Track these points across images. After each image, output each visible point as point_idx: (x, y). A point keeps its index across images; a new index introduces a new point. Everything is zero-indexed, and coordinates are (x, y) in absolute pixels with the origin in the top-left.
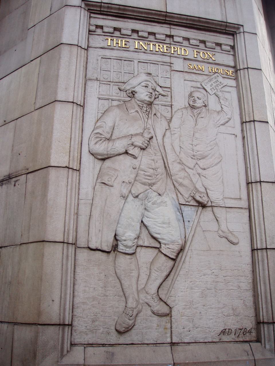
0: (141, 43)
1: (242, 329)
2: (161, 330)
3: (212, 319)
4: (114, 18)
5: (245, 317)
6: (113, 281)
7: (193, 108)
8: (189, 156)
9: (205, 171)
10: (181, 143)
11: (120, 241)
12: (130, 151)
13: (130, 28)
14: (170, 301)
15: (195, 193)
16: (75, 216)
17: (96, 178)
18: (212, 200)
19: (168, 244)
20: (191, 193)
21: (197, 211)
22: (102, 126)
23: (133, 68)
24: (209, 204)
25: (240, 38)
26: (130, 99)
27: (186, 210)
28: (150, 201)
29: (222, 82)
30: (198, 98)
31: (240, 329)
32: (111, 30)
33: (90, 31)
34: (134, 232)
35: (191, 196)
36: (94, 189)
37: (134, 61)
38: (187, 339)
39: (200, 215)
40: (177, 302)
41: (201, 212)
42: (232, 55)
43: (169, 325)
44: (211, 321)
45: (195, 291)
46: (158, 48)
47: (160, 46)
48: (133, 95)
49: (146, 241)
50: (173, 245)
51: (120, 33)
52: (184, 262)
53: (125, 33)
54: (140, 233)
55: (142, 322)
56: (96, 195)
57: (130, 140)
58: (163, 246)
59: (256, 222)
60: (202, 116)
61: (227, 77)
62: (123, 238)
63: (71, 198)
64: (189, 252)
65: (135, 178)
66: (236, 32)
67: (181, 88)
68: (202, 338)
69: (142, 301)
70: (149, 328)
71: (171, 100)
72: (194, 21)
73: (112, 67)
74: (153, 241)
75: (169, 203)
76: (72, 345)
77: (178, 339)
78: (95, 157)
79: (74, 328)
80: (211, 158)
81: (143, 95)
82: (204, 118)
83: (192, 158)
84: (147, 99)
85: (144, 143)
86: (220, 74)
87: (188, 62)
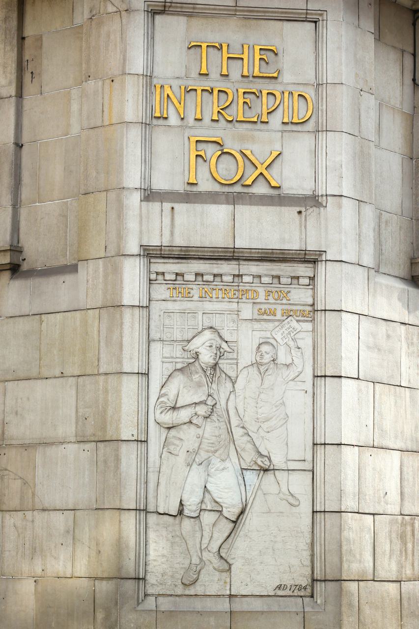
2: (222, 583)
3: (268, 575)
13: (194, 272)
16: (145, 485)
17: (162, 446)
18: (274, 464)
19: (229, 508)
22: (167, 393)
23: (197, 322)
24: (272, 467)
25: (321, 267)
30: (265, 352)
32: (173, 277)
33: (150, 280)
40: (236, 559)
41: (262, 476)
43: (228, 580)
44: (268, 577)
50: (234, 508)
56: (162, 463)
58: (224, 509)
61: (303, 319)
62: (188, 503)
63: (141, 469)
67: (246, 340)
72: (267, 253)
75: (231, 468)
76: (146, 595)
79: (147, 582)
81: (207, 357)
83: (256, 421)
86: (294, 316)
87: (258, 306)
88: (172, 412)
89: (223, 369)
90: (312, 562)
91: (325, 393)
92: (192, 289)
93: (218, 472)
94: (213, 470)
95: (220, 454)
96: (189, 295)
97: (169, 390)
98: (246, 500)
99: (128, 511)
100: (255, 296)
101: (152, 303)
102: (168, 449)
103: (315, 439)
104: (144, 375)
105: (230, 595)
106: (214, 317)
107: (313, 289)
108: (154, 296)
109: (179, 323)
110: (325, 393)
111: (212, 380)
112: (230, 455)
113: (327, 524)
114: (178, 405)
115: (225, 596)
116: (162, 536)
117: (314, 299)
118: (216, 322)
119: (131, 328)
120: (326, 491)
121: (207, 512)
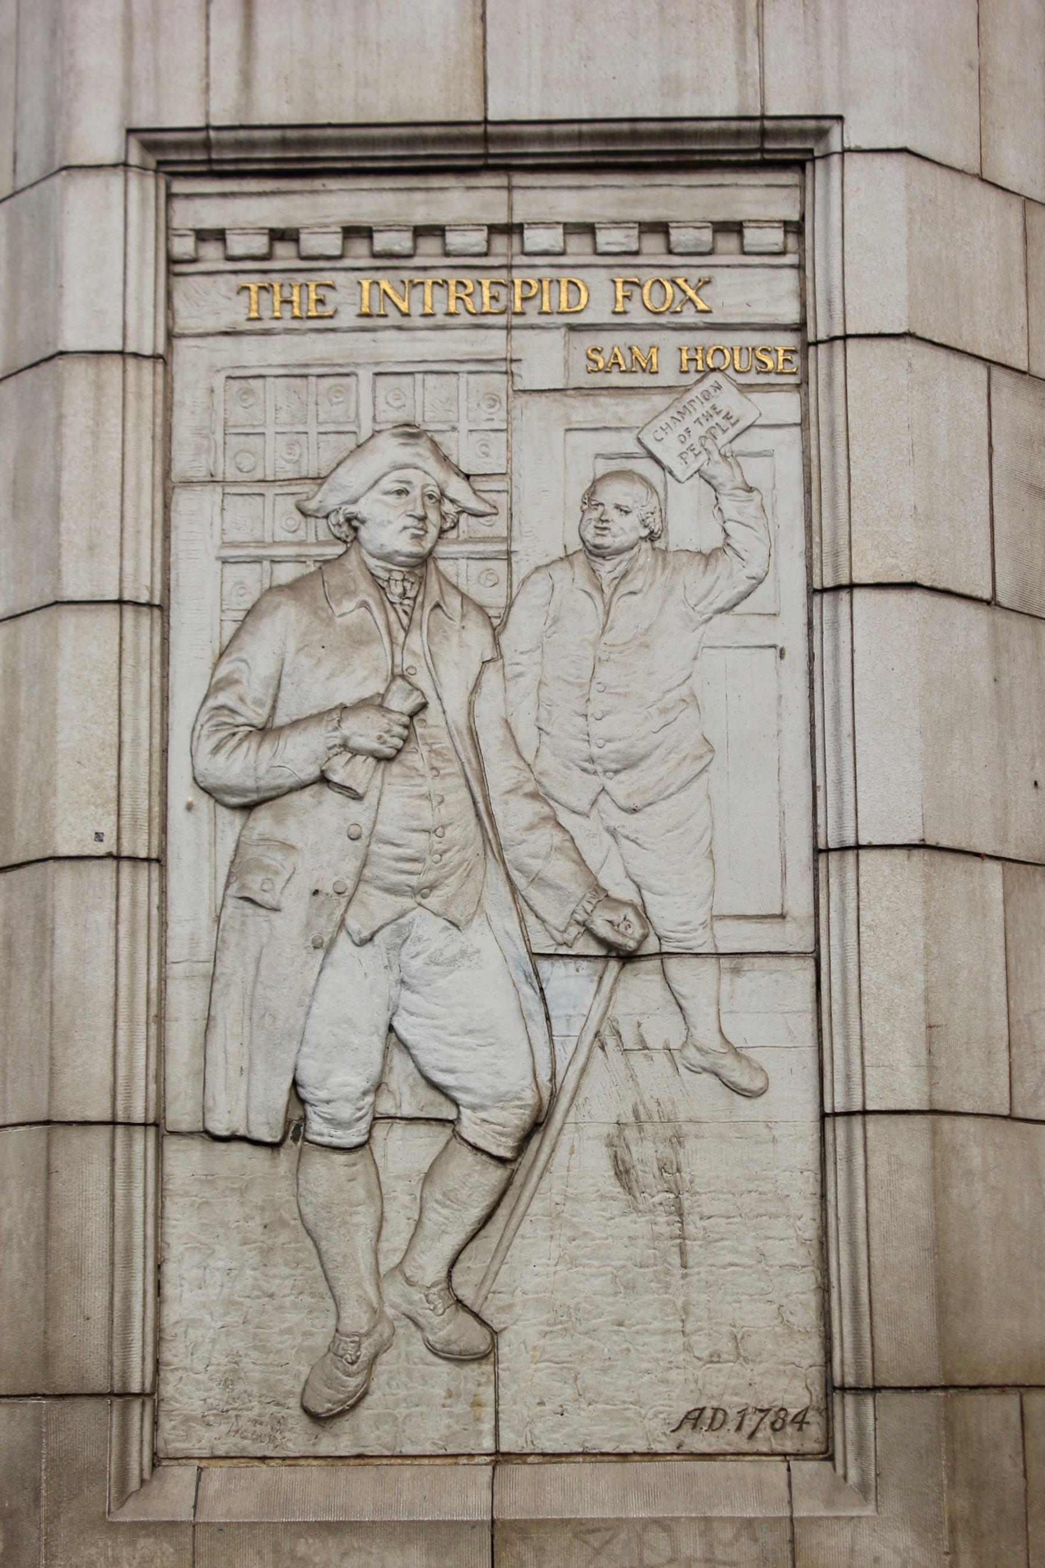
0: (385, 285)
1: (769, 1410)
2: (461, 1408)
3: (648, 1372)
4: (269, 185)
5: (782, 1367)
6: (293, 1245)
7: (597, 556)
8: (571, 765)
9: (636, 816)
10: (544, 715)
11: (312, 1105)
12: (334, 771)
14: (493, 1309)
15: (589, 908)
16: (153, 1028)
17: (222, 880)
18: (662, 932)
19: (483, 1107)
20: (574, 912)
21: (601, 978)
22: (236, 676)
23: (353, 405)
24: (651, 946)
25: (825, 178)
26: (340, 549)
27: (559, 977)
28: (417, 955)
29: (735, 414)
30: (618, 507)
31: (761, 1411)
32: (259, 244)
33: (172, 261)
34: (360, 1071)
35: (578, 923)
36: (218, 919)
37: (356, 375)
38: (556, 1441)
39: (613, 990)
40: (518, 1310)
41: (616, 980)
42: (792, 266)
43: (487, 1393)
44: (647, 1378)
45: (587, 1270)
46: (458, 298)
47: (465, 286)
48: (352, 532)
49: (407, 1098)
50: (502, 1108)
51: (298, 252)
52: (545, 1168)
53: (316, 251)
54: (383, 1071)
55: (394, 1383)
57: (336, 729)
58: (466, 1113)
59: (835, 1007)
60: (631, 588)
61: (762, 379)
62: (323, 1094)
64: (565, 1131)
65: (360, 874)
66: (811, 151)
67: (548, 471)
68: (610, 1440)
69: (393, 1311)
70: (416, 1401)
71: (510, 529)
73: (271, 413)
74: (427, 1095)
77: (521, 1442)
78: (217, 801)
79: (164, 1407)
80: (664, 761)
81: (390, 531)
82: (640, 596)
83: (584, 770)
84: (404, 545)
85: (386, 736)
86: (730, 372)
87: (589, 340)
88: (254, 746)
89: (454, 580)
90: (825, 1314)
91: (853, 651)
92: (331, 287)
93: (437, 969)
94: (418, 962)
95: (448, 902)
96: (321, 308)
97: (242, 665)
98: (554, 1075)
99: (81, 1128)
100: (573, 302)
101: (179, 344)
102: (243, 887)
103: (821, 831)
104: (145, 609)
105: (497, 1453)
106: (419, 383)
107: (800, 267)
108: (187, 318)
109: (284, 416)
110: (853, 651)
111: (411, 620)
112: (487, 905)
113: (873, 1161)
114: (281, 719)
115: (477, 1460)
116: (225, 1225)
117: (803, 306)
118: (427, 403)
119: (96, 431)
120: (866, 1030)
121: (399, 1128)
